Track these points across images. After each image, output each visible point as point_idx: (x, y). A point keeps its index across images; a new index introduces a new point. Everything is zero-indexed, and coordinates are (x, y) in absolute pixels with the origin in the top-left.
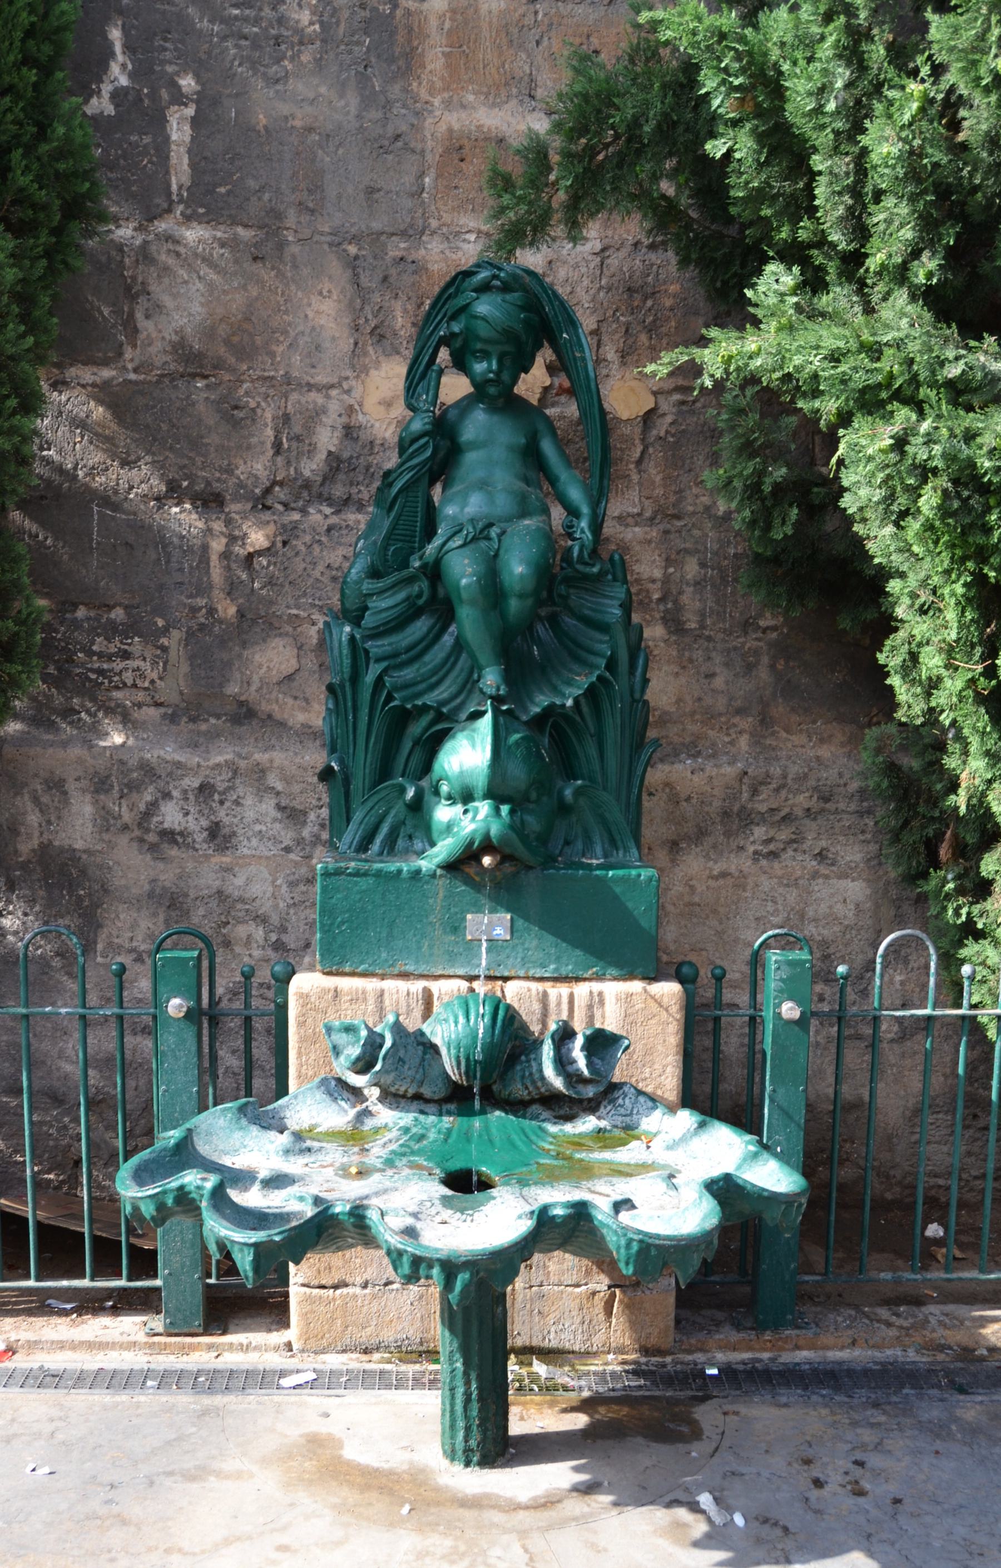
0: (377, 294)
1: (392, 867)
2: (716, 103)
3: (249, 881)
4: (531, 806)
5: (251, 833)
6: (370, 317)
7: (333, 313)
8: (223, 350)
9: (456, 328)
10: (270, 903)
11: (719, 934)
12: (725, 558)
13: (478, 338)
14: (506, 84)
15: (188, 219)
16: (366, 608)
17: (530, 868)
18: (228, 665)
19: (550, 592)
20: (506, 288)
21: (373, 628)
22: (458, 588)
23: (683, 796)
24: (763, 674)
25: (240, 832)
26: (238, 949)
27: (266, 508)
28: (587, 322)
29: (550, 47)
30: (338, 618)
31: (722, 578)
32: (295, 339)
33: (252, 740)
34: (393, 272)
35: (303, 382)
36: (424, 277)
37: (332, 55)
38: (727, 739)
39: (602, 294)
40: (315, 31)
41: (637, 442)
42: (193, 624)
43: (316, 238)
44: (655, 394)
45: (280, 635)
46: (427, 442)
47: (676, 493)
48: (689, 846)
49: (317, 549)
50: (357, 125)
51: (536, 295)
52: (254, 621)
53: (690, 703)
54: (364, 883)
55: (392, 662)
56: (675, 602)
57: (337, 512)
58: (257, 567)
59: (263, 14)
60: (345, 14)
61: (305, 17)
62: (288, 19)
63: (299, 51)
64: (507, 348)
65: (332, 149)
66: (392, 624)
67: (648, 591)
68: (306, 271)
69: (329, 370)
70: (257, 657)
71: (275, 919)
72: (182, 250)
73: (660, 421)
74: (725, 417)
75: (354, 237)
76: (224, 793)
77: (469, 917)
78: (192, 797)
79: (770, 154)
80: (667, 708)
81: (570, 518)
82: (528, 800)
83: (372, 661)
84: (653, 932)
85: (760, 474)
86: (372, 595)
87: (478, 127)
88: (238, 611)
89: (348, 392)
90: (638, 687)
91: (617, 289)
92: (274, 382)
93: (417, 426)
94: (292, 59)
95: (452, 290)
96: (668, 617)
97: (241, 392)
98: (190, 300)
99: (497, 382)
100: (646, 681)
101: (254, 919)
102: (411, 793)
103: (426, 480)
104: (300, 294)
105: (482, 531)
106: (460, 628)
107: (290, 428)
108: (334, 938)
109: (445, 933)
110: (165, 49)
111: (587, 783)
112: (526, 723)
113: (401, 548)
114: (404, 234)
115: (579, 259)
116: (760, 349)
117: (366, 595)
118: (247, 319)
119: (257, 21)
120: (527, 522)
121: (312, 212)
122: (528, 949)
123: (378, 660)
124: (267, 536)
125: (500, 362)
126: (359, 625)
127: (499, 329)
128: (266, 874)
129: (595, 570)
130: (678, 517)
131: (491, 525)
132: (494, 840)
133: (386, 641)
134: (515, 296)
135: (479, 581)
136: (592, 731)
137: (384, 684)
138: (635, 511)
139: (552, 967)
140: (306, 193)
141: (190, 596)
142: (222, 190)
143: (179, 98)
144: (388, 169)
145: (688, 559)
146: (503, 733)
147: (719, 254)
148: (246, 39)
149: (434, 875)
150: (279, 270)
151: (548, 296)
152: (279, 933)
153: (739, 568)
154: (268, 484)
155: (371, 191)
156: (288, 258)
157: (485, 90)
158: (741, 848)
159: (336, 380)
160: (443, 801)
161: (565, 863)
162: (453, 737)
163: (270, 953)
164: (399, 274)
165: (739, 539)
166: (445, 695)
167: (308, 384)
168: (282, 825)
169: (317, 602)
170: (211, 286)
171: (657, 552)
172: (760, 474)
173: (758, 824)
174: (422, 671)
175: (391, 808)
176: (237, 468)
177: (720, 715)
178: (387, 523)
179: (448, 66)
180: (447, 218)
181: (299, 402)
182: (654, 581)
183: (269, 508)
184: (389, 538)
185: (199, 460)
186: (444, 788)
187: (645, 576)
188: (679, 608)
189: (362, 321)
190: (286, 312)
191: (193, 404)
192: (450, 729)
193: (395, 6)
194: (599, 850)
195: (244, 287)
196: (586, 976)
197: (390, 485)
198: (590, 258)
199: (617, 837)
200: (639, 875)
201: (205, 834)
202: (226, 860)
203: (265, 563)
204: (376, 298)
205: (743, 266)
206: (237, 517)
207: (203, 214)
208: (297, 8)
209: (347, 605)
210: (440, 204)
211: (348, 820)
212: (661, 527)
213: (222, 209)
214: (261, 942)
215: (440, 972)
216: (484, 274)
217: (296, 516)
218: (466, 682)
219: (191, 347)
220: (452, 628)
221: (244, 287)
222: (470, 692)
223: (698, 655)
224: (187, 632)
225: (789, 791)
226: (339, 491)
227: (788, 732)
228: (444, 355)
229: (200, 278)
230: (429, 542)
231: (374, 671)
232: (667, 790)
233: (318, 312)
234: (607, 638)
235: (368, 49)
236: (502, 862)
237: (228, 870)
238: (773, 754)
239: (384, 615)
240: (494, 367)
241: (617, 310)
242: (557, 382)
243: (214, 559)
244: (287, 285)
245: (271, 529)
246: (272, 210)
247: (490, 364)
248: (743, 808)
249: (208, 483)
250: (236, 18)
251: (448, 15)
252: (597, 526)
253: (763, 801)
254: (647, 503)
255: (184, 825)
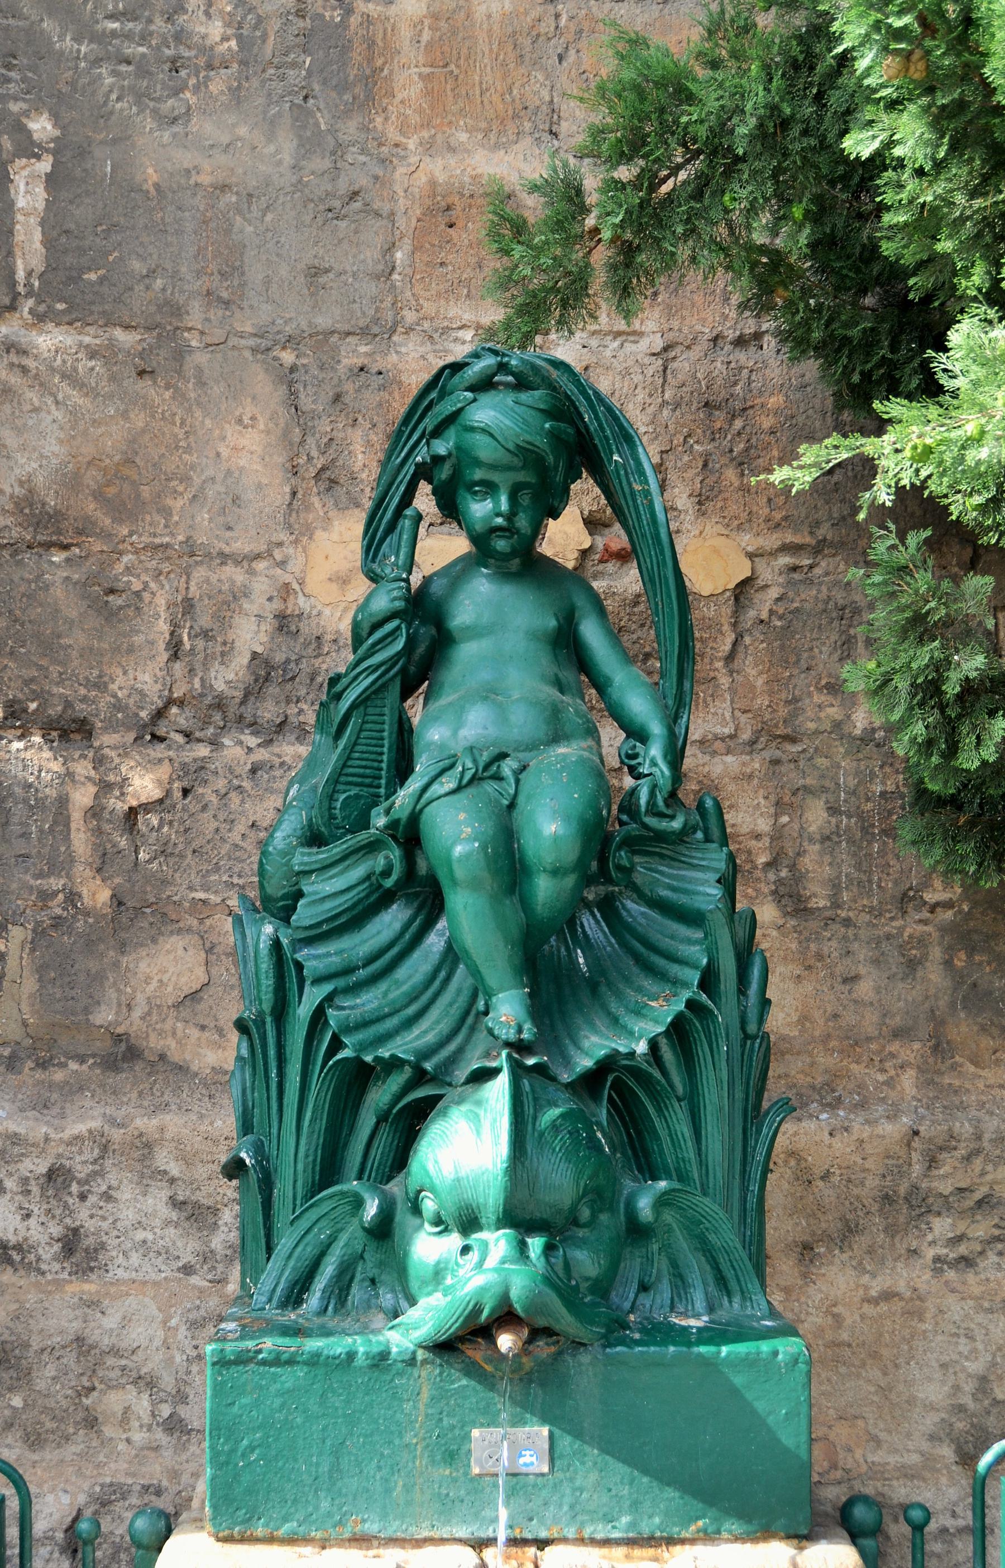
0: (325, 421)
1: (337, 1346)
2: (861, 65)
3: (126, 1321)
4: (581, 1233)
5: (129, 1245)
6: (314, 453)
7: (259, 450)
8: (92, 506)
9: (441, 447)
10: (159, 1356)
11: (884, 1391)
12: (868, 799)
13: (478, 463)
14: (515, 116)
15: (40, 318)
16: (300, 894)
17: (579, 1345)
18: (98, 978)
19: (603, 859)
20: (521, 384)
21: (311, 927)
22: (448, 861)
23: (818, 1172)
24: (934, 974)
25: (113, 1242)
26: (108, 1431)
27: (157, 738)
28: (649, 453)
29: (579, 63)
30: (256, 910)
31: (863, 828)
32: (202, 488)
33: (134, 1095)
34: (349, 387)
35: (214, 552)
36: (396, 394)
37: (255, 82)
38: (881, 1078)
39: (666, 413)
40: (229, 49)
41: (726, 628)
42: (44, 917)
43: (233, 341)
44: (751, 556)
45: (179, 931)
46: (398, 628)
47: (788, 702)
48: (830, 1251)
49: (235, 798)
50: (294, 179)
51: (568, 397)
52: (138, 911)
53: (821, 1022)
54: (290, 1377)
55: (341, 983)
56: (792, 867)
57: (268, 743)
58: (141, 826)
59: (153, 28)
60: (275, 25)
61: (215, 30)
62: (190, 34)
63: (206, 77)
64: (522, 477)
65: (256, 213)
66: (342, 920)
67: (749, 852)
68: (217, 390)
69: (254, 532)
70: (143, 966)
71: (168, 1382)
72: (30, 363)
73: (759, 596)
74: (877, 579)
75: (290, 339)
76: (87, 1182)
77: (475, 1433)
78: (35, 1189)
79: (953, 148)
80: (786, 1031)
81: (632, 742)
82: (575, 1222)
83: (308, 983)
84: (803, 1454)
85: (940, 667)
86: (312, 872)
87: (474, 178)
88: (113, 896)
89: (282, 564)
90: (752, 1014)
91: (689, 404)
92: (169, 552)
93: (383, 603)
94: (197, 89)
95: (434, 395)
96: (782, 890)
97: (119, 568)
98: (42, 435)
99: (508, 530)
100: (765, 1003)
101: (135, 1383)
102: (371, 1209)
103: (396, 688)
104: (208, 422)
105: (487, 767)
106: (452, 925)
107: (192, 619)
108: (236, 1476)
109: (433, 1462)
110: (8, 80)
111: (677, 1185)
112: (570, 1086)
113: (357, 797)
114: (365, 333)
115: (630, 363)
116: (983, 433)
117: (298, 873)
118: (129, 462)
119: (144, 38)
120: (562, 750)
121: (227, 303)
122: (582, 1490)
123: (318, 981)
124: (159, 782)
125: (513, 498)
126: (286, 920)
127: (511, 446)
128: (153, 1309)
129: (677, 824)
130: (793, 740)
131: (503, 756)
132: (518, 1308)
133: (331, 947)
134: (535, 397)
135: (484, 847)
136: (680, 1090)
137: (326, 1022)
138: (727, 731)
139: (625, 1520)
140: (217, 277)
141: (40, 875)
142: (93, 276)
143: (29, 149)
144: (340, 241)
145: (810, 801)
146: (529, 1110)
147: (855, 332)
148: (129, 63)
149: (411, 1361)
150: (177, 389)
151: (588, 398)
152: (175, 1404)
153: (890, 813)
154: (160, 704)
155: (315, 272)
156: (189, 370)
157: (483, 125)
158: (915, 1252)
159: (263, 548)
160: (427, 1226)
161: (643, 1330)
162: (444, 1113)
163: (160, 1436)
164: (358, 391)
165: (888, 769)
166: (430, 1038)
167: (221, 554)
168: (179, 1231)
169: (236, 880)
170: (74, 413)
171: (761, 792)
172: (940, 667)
173: (939, 1214)
174: (392, 996)
175: (341, 1230)
176: (113, 681)
177: (869, 1039)
178: (332, 759)
179: (428, 93)
180: (429, 308)
181: (207, 581)
182: (758, 837)
183: (162, 739)
184: (335, 781)
185: (54, 670)
186: (429, 1205)
187: (744, 829)
188: (798, 877)
189: (302, 460)
190: (188, 450)
191: (47, 587)
192: (439, 1098)
193: (349, 11)
194: (700, 1305)
195: (125, 415)
196: (684, 1534)
197: (338, 697)
198: (647, 360)
199: (729, 1274)
200: (776, 1353)
201: (57, 1247)
202: (90, 1287)
203: (155, 822)
204: (324, 426)
205: (894, 348)
206: (113, 754)
207: (63, 311)
208: (203, 18)
209: (269, 890)
210: (418, 289)
211: (269, 1250)
212: (767, 754)
213: (93, 303)
214: (146, 1419)
215: (425, 1534)
216: (479, 367)
217: (203, 751)
218: (467, 1013)
219: (44, 505)
220: (441, 924)
221: (125, 415)
222: (473, 1029)
223: (832, 947)
224: (34, 931)
225: (987, 1160)
226: (268, 711)
227: (976, 1064)
228: (425, 501)
229: (57, 403)
230: (402, 784)
231: (313, 996)
232: (793, 1163)
233: (235, 448)
234: (699, 935)
235: (310, 72)
236: (530, 1341)
237: (92, 1304)
238: (956, 1100)
239: (328, 905)
240: (504, 505)
241: (690, 435)
242: (600, 542)
243: (77, 817)
244: (189, 410)
245: (164, 771)
246: (167, 302)
247: (497, 503)
248: (915, 1187)
249: (68, 705)
250: (114, 33)
251: (427, 22)
252: (675, 756)
253: (945, 1177)
254: (743, 719)
255: (22, 1233)
